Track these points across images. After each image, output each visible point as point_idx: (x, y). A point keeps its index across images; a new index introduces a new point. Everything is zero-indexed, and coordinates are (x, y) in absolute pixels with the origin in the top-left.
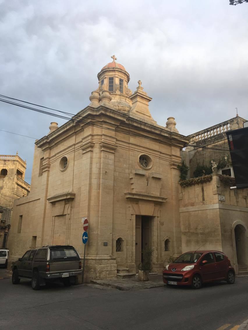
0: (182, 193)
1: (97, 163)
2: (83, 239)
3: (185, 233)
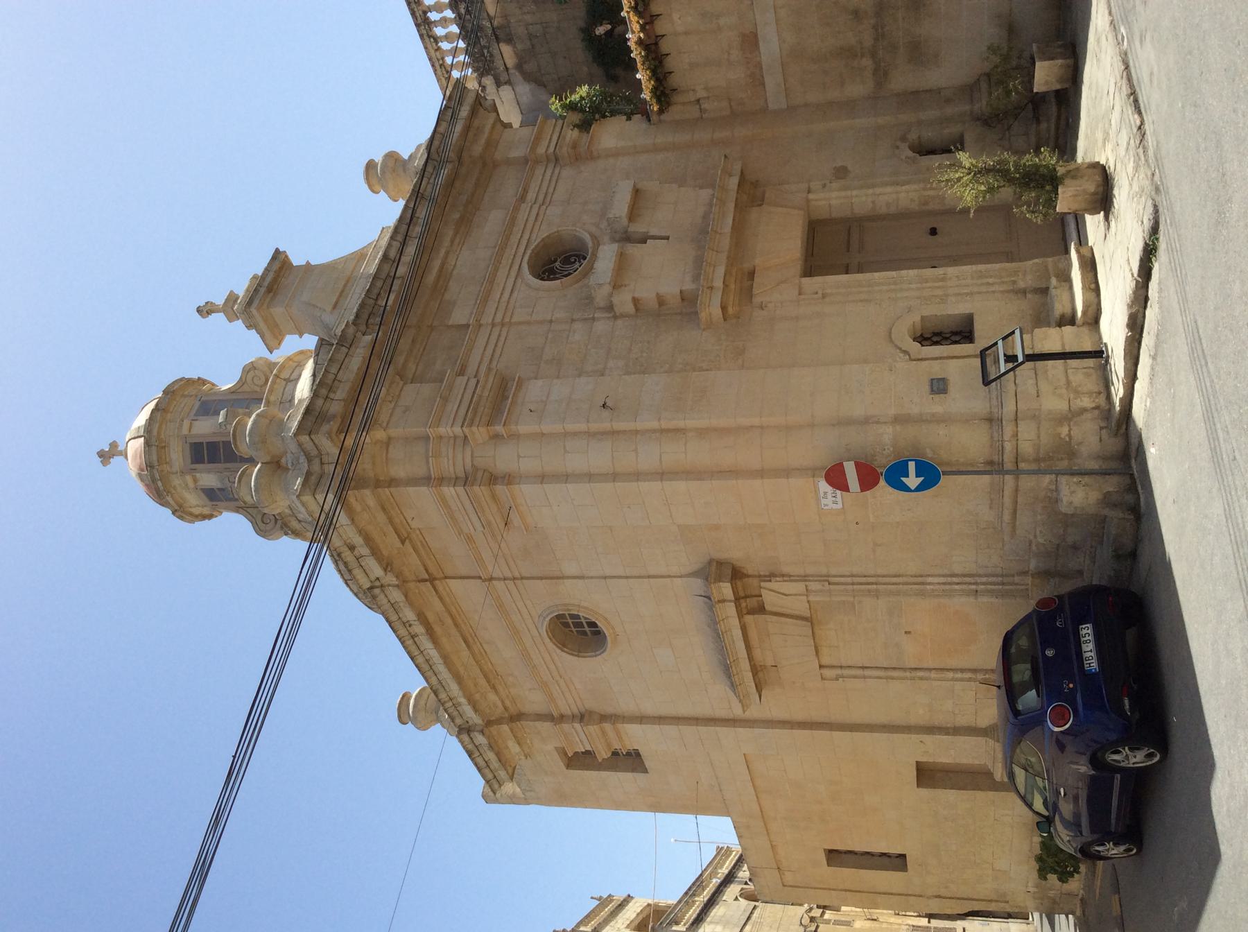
0: (698, 101)
1: (566, 451)
2: (920, 488)
3: (881, 74)
